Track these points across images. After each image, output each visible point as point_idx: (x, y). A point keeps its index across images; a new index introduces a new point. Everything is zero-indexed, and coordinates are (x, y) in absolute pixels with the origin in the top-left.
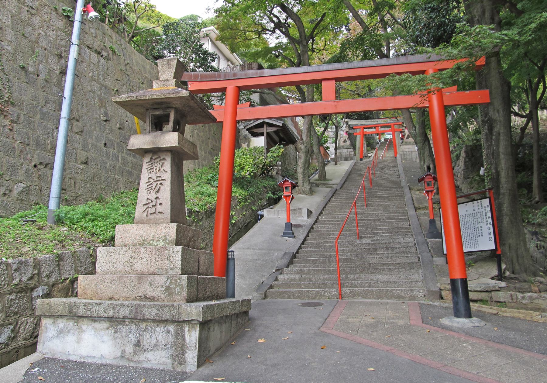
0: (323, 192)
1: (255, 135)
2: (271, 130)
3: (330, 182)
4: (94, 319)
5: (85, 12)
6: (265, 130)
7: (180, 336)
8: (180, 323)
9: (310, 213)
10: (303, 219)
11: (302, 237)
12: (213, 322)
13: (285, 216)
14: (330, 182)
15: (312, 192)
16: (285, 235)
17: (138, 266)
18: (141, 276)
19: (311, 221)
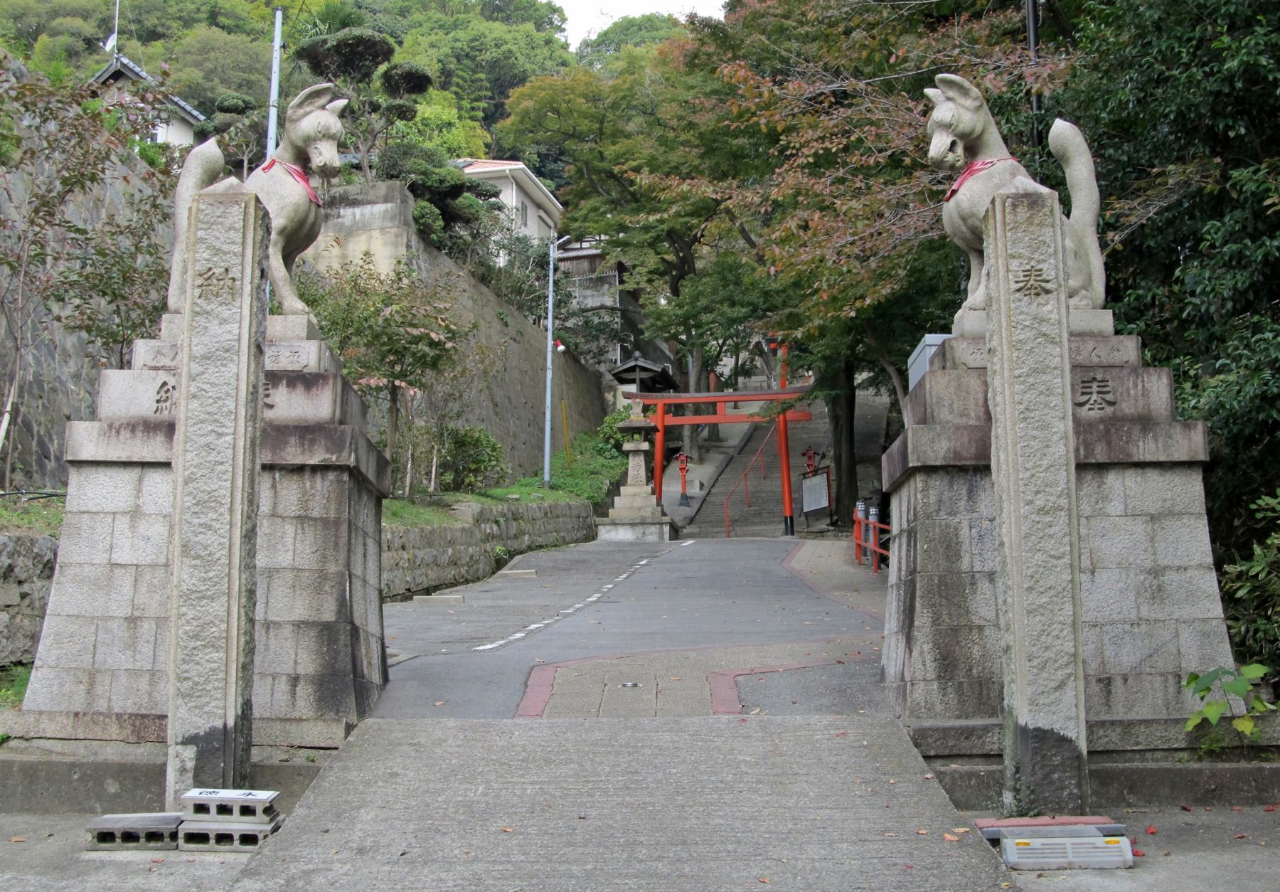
0: (716, 459)
1: (623, 381)
2: (645, 375)
3: (725, 444)
4: (623, 524)
5: (556, 346)
6: (638, 375)
7: (661, 529)
8: (661, 524)
9: (702, 485)
10: (695, 491)
11: (696, 507)
12: (1008, 177)
13: (680, 489)
14: (725, 444)
15: (701, 460)
16: (681, 504)
17: (636, 505)
18: (639, 509)
19: (704, 493)
